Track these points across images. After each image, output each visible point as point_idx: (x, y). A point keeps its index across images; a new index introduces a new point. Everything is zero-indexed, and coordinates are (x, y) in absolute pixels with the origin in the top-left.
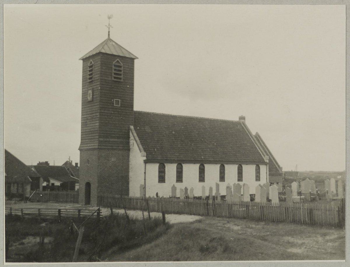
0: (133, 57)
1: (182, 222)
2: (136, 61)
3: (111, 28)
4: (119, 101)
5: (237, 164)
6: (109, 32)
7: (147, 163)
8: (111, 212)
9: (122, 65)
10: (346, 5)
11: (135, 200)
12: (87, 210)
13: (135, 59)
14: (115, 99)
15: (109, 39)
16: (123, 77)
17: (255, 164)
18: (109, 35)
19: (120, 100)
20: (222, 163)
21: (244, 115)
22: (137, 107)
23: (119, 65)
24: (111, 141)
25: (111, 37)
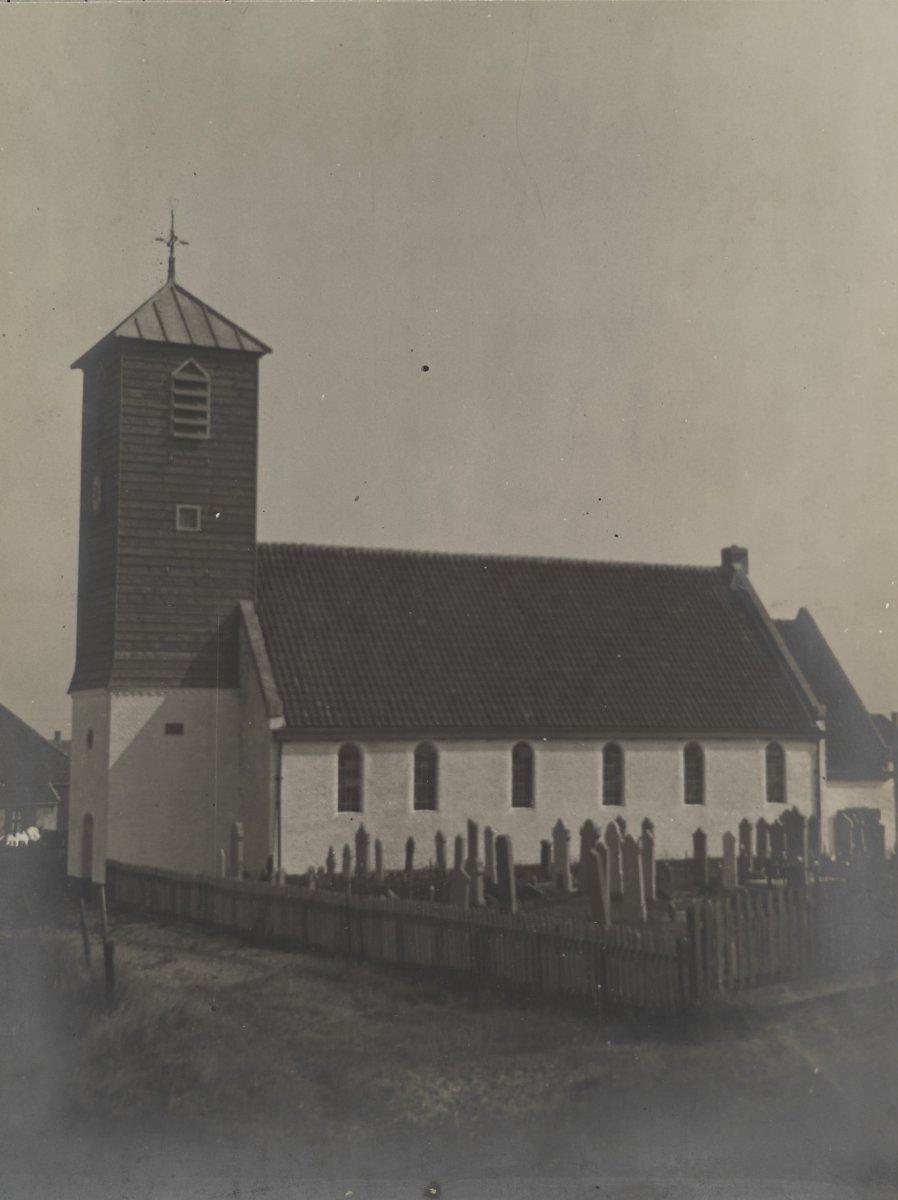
0: (249, 346)
2: (264, 363)
4: (195, 511)
6: (172, 261)
7: (286, 741)
9: (207, 376)
12: (87, 952)
13: (258, 355)
14: (180, 503)
15: (176, 289)
16: (212, 422)
18: (171, 272)
19: (199, 508)
21: (741, 544)
22: (274, 525)
23: (196, 378)
24: (165, 661)
25: (181, 279)
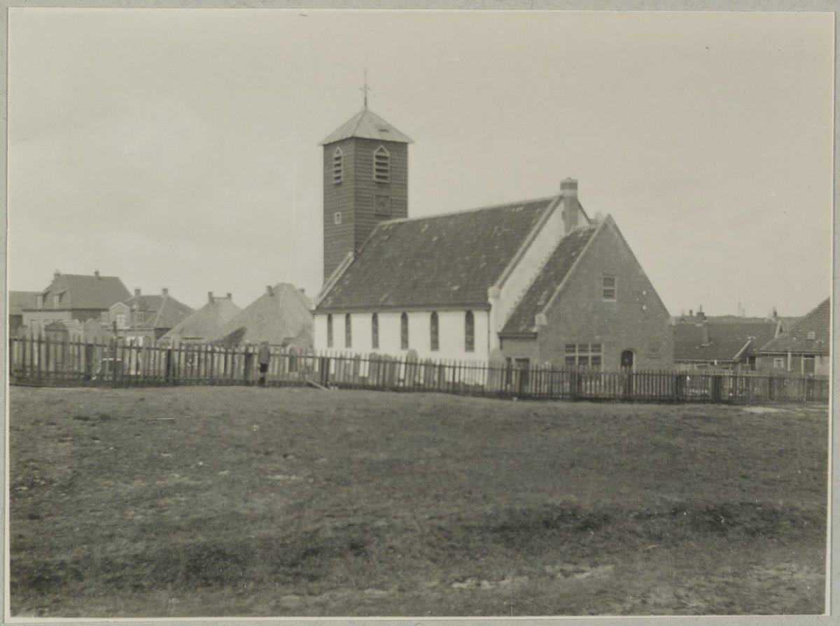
0: (406, 141)
1: (371, 391)
3: (369, 92)
5: (428, 311)
6: (366, 99)
8: (723, 398)
10: (836, 13)
11: (775, 381)
17: (370, 312)
18: (366, 104)
20: (468, 308)
23: (383, 154)
